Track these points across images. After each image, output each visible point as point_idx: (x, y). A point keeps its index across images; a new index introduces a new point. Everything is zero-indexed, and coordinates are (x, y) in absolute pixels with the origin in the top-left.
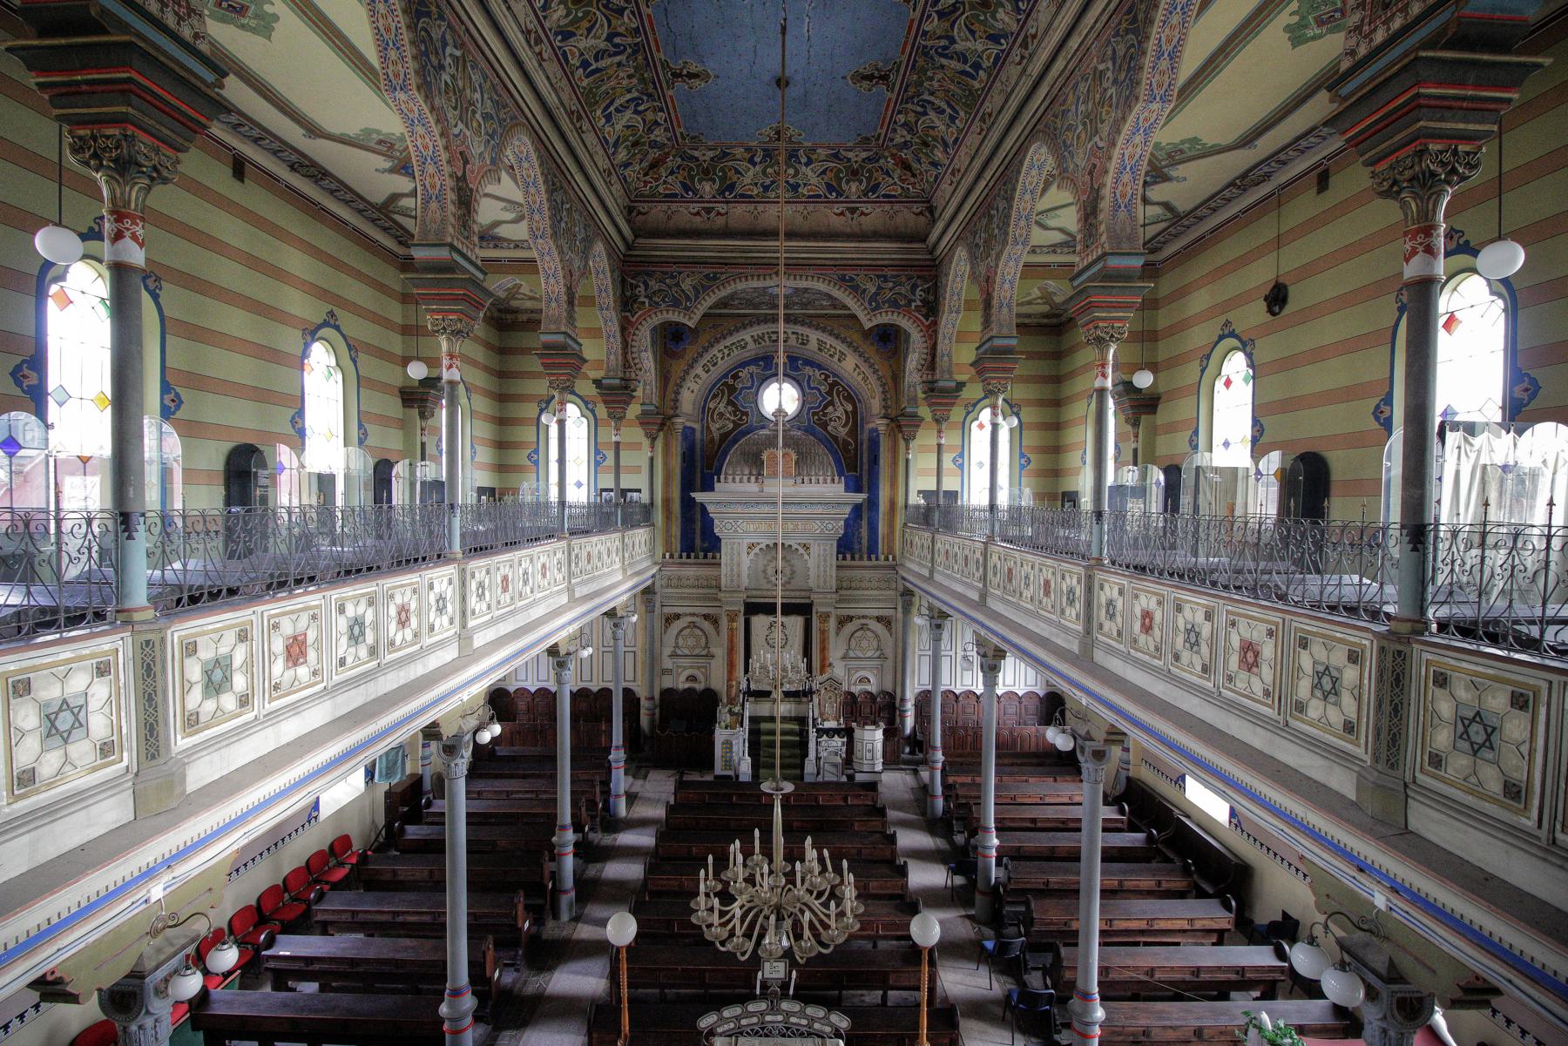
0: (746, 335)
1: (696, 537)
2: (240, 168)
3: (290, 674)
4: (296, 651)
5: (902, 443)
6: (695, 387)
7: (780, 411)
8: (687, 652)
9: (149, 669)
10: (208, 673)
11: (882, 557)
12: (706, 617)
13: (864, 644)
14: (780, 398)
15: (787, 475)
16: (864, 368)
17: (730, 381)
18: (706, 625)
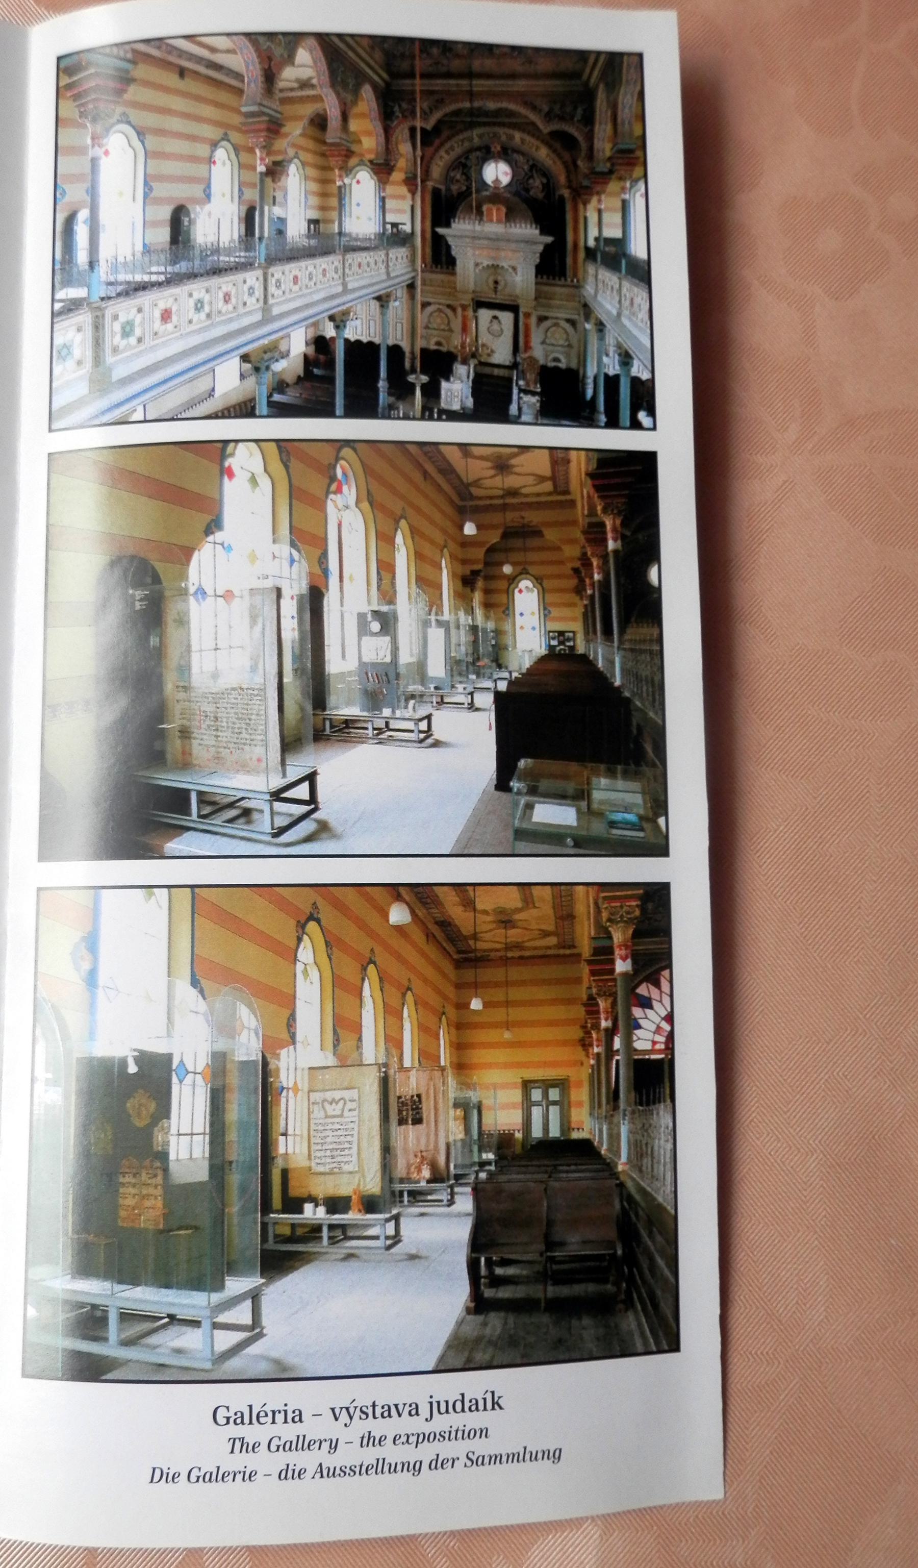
0: (476, 132)
1: (441, 256)
2: (182, 73)
3: (163, 327)
4: (166, 316)
5: (581, 206)
7: (497, 181)
9: (98, 327)
10: (123, 328)
12: (449, 306)
13: (557, 336)
14: (497, 173)
15: (499, 221)
16: (553, 155)
17: (463, 160)
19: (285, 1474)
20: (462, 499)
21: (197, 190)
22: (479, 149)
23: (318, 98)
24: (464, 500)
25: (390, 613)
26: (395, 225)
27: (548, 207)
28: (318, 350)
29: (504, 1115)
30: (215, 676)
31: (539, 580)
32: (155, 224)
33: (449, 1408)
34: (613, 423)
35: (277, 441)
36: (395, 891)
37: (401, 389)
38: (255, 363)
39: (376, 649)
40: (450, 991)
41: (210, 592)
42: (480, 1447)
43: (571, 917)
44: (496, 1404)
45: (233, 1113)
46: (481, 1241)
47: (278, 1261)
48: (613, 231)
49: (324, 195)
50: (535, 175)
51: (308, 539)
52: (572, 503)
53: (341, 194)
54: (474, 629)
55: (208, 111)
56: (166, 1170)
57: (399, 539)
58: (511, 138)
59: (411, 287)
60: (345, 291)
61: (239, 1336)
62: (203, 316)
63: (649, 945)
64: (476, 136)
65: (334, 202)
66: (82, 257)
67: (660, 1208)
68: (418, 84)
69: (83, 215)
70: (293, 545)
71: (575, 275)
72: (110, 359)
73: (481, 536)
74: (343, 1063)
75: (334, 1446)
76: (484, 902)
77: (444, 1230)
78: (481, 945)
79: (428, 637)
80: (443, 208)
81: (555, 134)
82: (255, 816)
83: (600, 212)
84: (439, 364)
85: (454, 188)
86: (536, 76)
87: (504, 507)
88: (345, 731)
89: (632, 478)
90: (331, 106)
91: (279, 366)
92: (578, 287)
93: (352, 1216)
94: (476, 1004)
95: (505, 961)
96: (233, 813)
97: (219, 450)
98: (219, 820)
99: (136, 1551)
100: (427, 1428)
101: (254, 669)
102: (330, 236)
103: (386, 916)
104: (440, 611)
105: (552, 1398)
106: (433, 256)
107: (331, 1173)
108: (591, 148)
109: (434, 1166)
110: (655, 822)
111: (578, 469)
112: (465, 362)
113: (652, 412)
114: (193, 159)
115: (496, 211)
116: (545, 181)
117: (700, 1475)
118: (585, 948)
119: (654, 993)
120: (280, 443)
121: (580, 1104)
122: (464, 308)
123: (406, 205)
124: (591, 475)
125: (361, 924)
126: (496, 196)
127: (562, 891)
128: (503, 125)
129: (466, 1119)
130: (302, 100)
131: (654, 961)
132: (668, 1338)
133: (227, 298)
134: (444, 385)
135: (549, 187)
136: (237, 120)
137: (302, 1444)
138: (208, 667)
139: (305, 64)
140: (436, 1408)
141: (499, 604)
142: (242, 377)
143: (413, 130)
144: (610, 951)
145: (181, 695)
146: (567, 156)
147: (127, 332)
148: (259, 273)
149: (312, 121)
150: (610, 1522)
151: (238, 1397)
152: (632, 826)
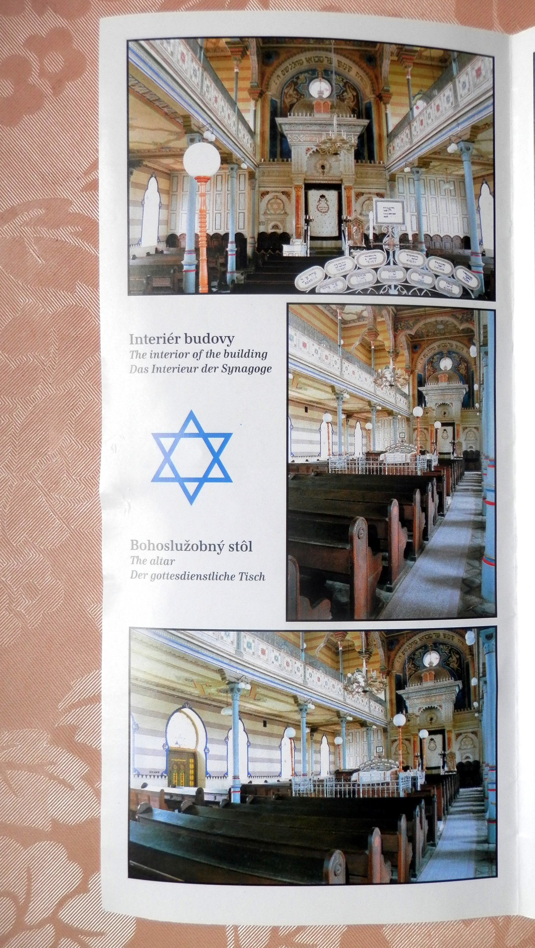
5: (383, 106)
6: (400, 660)
8: (272, 212)
11: (377, 162)
12: (283, 193)
14: (319, 89)
16: (361, 73)
18: (284, 197)
50: (348, 90)
106: (271, 135)
116: (458, 656)
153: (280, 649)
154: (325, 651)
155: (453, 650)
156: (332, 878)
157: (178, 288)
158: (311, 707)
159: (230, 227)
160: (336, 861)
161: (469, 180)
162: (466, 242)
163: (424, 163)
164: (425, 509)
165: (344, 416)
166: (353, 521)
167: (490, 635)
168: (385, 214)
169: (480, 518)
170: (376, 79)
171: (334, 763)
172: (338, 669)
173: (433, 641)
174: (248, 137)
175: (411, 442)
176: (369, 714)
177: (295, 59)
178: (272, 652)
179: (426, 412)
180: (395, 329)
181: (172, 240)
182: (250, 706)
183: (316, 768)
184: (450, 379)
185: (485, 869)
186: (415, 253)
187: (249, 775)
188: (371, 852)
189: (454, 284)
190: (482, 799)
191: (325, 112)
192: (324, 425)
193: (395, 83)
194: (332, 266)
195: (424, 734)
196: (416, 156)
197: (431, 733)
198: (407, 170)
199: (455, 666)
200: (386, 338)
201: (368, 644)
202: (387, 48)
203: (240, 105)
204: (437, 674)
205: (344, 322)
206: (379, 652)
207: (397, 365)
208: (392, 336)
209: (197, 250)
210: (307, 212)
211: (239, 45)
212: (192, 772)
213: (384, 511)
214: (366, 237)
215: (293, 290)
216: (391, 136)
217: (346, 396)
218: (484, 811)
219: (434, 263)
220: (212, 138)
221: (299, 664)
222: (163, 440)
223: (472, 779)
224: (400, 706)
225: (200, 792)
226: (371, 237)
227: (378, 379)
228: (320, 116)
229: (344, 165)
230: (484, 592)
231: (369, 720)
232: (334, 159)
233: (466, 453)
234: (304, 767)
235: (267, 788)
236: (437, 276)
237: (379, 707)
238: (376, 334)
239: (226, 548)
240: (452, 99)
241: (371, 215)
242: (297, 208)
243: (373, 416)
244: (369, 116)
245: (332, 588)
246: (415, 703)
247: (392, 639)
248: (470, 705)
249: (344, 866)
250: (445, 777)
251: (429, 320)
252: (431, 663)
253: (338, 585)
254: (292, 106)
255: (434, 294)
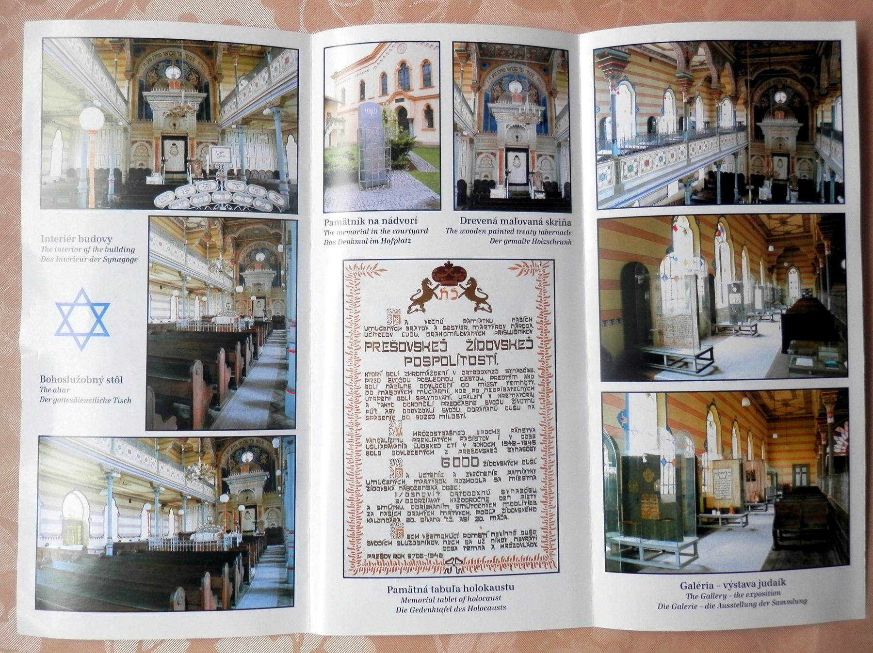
0: (772, 80)
1: (758, 135)
2: (651, 59)
4: (647, 163)
14: (172, 73)
16: (202, 62)
19: (708, 606)
20: (768, 236)
21: (659, 110)
22: (773, 87)
23: (708, 69)
24: (769, 237)
25: (740, 284)
26: (740, 123)
27: (801, 110)
28: (710, 177)
29: (786, 477)
30: (672, 310)
31: (798, 268)
32: (641, 124)
33: (766, 584)
34: (828, 202)
35: (694, 215)
36: (744, 393)
37: (743, 193)
38: (685, 183)
39: (735, 299)
40: (765, 431)
41: (669, 276)
42: (778, 598)
43: (811, 402)
44: (783, 583)
45: (684, 477)
46: (778, 523)
47: (703, 531)
48: (828, 120)
49: (711, 111)
51: (708, 254)
52: (811, 236)
53: (718, 110)
54: (773, 289)
55: (662, 76)
56: (659, 498)
57: (743, 254)
58: (786, 81)
59: (747, 149)
60: (721, 152)
61: (689, 558)
62: (662, 163)
63: (841, 412)
64: (772, 81)
65: (715, 114)
66: (609, 137)
67: (844, 512)
68: (749, 60)
69: (609, 119)
70: (702, 257)
71: (812, 139)
72: (623, 181)
73: (774, 249)
74: (726, 459)
75: (725, 597)
76: (778, 397)
77: (764, 520)
78: (777, 414)
79: (755, 294)
80: (759, 114)
81: (803, 78)
82: (689, 365)
83: (822, 112)
84: (758, 181)
85: (763, 105)
86: (796, 54)
87: (785, 239)
88: (723, 332)
89: (834, 225)
90: (713, 73)
91: (694, 184)
92: (814, 144)
93: (730, 515)
94: (775, 436)
95: (786, 419)
96: (681, 364)
97: (671, 219)
98: (675, 366)
99: (674, 632)
100: (758, 591)
101: (687, 307)
102: (714, 129)
103: (741, 403)
104: (760, 283)
105: (801, 581)
107: (722, 499)
108: (819, 84)
109: (760, 497)
110: (843, 364)
111: (814, 221)
112: (768, 179)
113: (843, 196)
114: (656, 97)
115: (780, 114)
117: (857, 609)
118: (816, 415)
119: (842, 430)
120: (696, 216)
121: (814, 473)
122: (768, 156)
123: (744, 114)
124: (819, 224)
125: (731, 406)
126: (780, 107)
127: (808, 392)
128: (782, 76)
129: (772, 479)
130: (701, 70)
131: (842, 418)
132: (845, 560)
133: (672, 156)
134: (760, 189)
135: (802, 101)
136: (675, 80)
137: (713, 596)
138: (669, 307)
139: (702, 55)
140: (762, 584)
141: (783, 279)
142: (680, 189)
143: (746, 81)
144: (825, 415)
145: (659, 318)
146: (809, 88)
147: (630, 169)
148: (685, 145)
149: (705, 79)
150: (823, 626)
151: (690, 579)
152: (834, 366)
153: (141, 450)
154: (172, 451)
155: (263, 451)
156: (176, 607)
157: (75, 205)
158: (162, 489)
159: (110, 164)
160: (179, 595)
161: (278, 133)
162: (276, 175)
163: (246, 122)
164: (244, 355)
165: (187, 292)
166: (192, 363)
167: (291, 441)
168: (218, 156)
169: (284, 361)
170: (212, 66)
171: (178, 528)
172: (181, 463)
173: (249, 445)
174: (123, 104)
175: (234, 309)
176: (203, 494)
177: (157, 53)
178: (135, 452)
179: (245, 289)
180: (224, 234)
181: (71, 172)
182: (121, 489)
183: (165, 531)
184: (263, 267)
185: (286, 601)
186: (238, 182)
187: (119, 536)
188: (203, 589)
189: (268, 203)
190: (284, 553)
191: (176, 88)
192: (173, 298)
193: (226, 69)
194: (180, 191)
195: (242, 508)
196: (240, 118)
197: (246, 507)
198: (234, 126)
199: (265, 462)
200: (217, 239)
201: (202, 447)
202: (220, 45)
203: (118, 83)
204: (251, 467)
205: (188, 228)
206: (211, 452)
207: (225, 258)
208: (221, 239)
209: (88, 179)
210: (163, 155)
211: (118, 43)
212: (79, 535)
213: (215, 357)
214: (204, 172)
215: (154, 207)
216: (223, 104)
217: (189, 278)
218: (285, 562)
219: (252, 188)
220: (99, 104)
221: (154, 460)
222: (63, 308)
223: (277, 540)
224: (225, 489)
225: (85, 548)
226: (208, 172)
227: (212, 267)
228: (173, 91)
229: (189, 123)
230: (287, 412)
231: (203, 498)
232: (182, 119)
233: (274, 317)
234: (157, 531)
235: (131, 545)
236: (254, 198)
237: (210, 489)
238: (211, 237)
239: (105, 381)
240: (267, 79)
241: (207, 157)
242: (156, 152)
243: (208, 292)
244: (207, 91)
245: (177, 408)
246: (236, 487)
247: (219, 444)
248: (275, 489)
249: (184, 598)
250: (257, 538)
251: (248, 227)
252: (247, 460)
253: (182, 406)
254: (154, 84)
255: (252, 209)
